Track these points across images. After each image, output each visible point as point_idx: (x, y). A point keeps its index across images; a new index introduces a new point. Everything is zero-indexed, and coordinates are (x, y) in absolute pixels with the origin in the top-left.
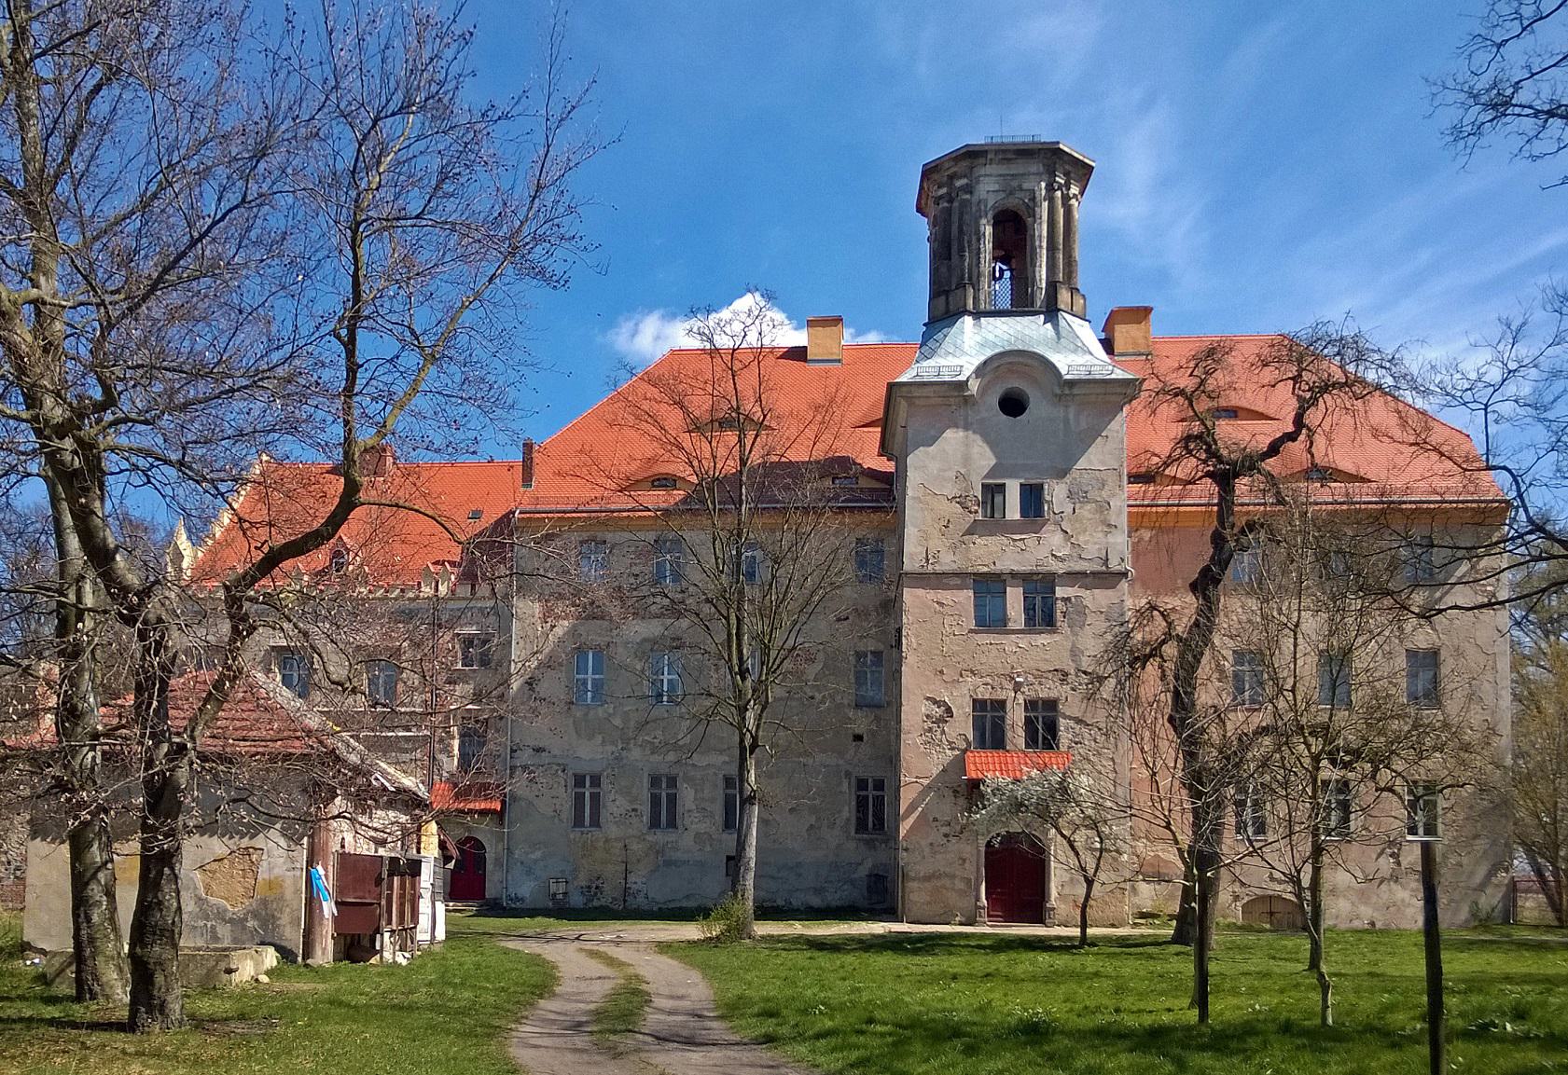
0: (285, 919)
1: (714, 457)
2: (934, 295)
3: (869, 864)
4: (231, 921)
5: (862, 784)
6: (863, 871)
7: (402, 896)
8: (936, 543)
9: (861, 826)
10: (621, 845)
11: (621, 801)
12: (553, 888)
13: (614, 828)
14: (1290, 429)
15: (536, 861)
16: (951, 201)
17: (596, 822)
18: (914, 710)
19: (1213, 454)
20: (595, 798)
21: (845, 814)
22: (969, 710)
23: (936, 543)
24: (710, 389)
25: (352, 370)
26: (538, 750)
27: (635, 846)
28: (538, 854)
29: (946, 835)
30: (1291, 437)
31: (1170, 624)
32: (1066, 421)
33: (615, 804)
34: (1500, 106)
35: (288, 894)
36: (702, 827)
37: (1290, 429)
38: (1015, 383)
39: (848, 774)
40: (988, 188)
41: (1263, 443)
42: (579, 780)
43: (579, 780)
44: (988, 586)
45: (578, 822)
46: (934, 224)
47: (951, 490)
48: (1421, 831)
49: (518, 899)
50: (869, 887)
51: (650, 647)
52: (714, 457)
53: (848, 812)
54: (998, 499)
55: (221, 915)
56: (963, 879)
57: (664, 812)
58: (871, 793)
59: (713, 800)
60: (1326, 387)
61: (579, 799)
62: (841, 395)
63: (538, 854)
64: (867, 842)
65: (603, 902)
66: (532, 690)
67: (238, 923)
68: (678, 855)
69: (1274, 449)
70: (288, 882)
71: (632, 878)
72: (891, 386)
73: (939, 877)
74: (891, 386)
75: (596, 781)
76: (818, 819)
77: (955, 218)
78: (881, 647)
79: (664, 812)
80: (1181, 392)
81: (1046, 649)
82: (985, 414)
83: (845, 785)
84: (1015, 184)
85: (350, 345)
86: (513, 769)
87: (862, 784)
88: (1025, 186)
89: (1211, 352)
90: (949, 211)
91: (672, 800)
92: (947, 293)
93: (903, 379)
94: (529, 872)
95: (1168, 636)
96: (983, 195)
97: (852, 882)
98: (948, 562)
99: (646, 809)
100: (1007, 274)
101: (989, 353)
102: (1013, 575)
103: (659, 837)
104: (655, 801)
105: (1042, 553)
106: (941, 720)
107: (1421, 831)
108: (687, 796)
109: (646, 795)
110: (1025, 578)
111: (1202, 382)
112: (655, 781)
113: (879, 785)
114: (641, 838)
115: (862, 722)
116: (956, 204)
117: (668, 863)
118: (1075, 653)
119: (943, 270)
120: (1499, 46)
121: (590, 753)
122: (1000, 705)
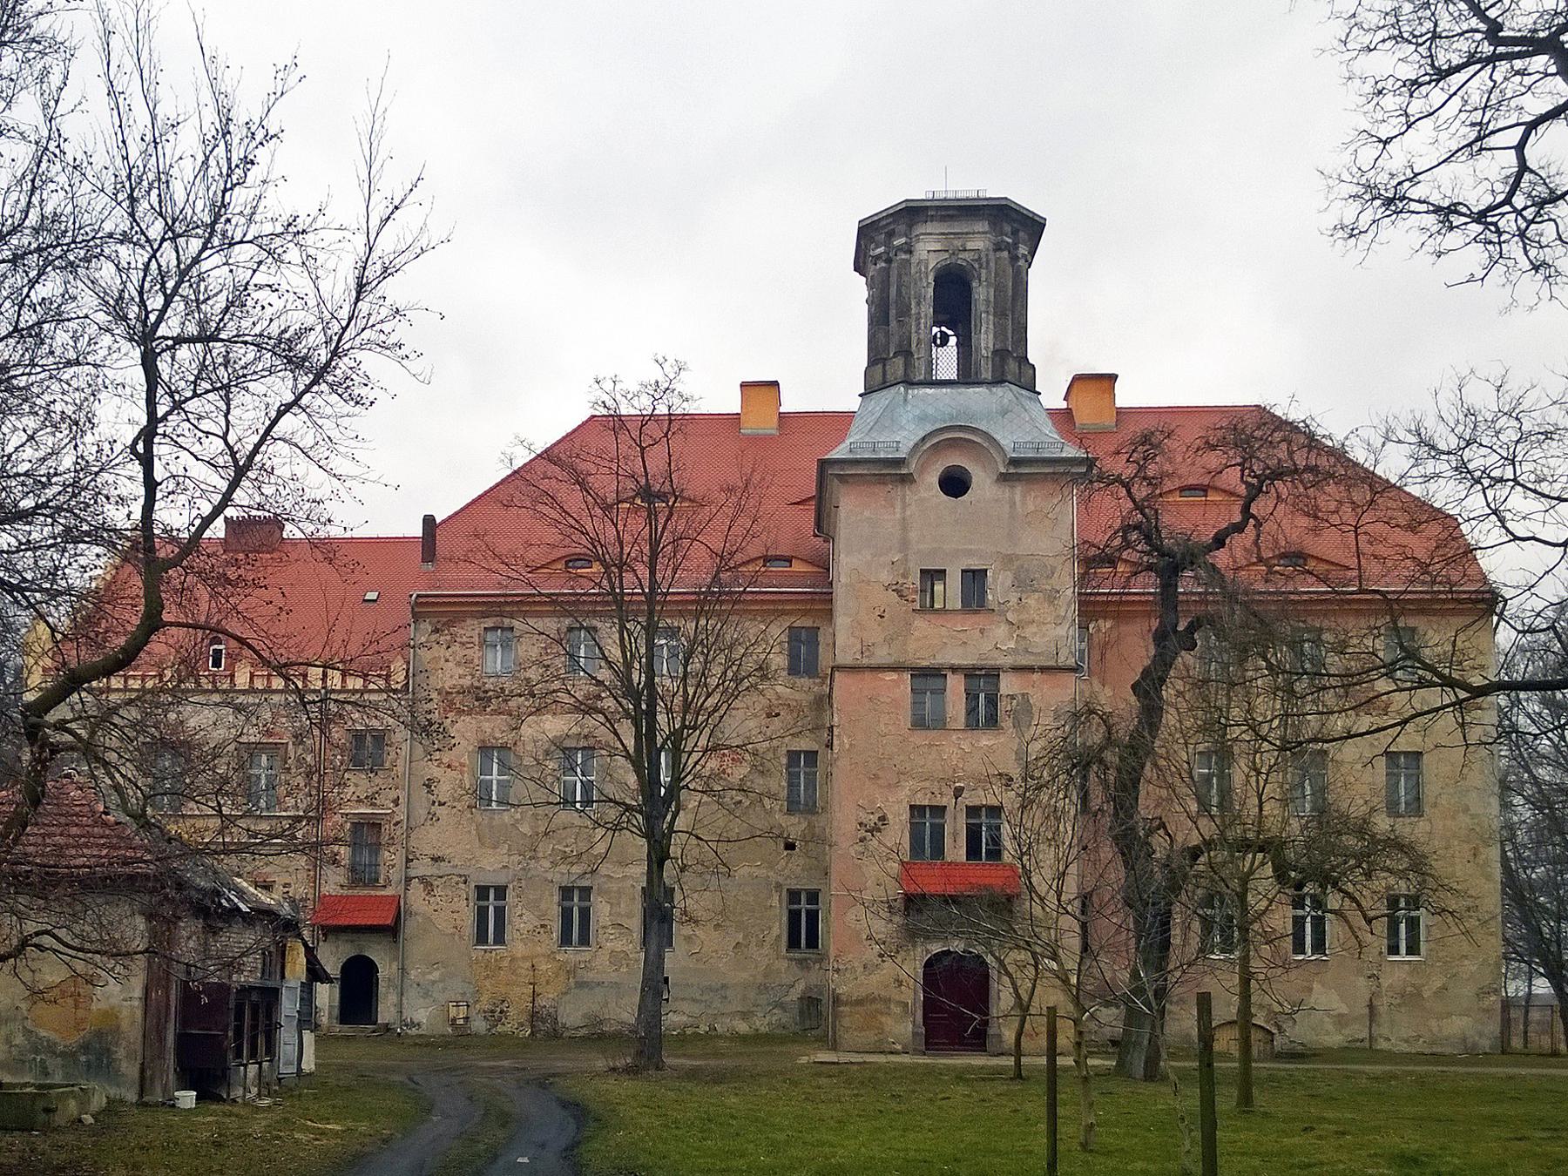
0: (121, 1053)
1: (621, 544)
2: (872, 362)
3: (800, 986)
4: (63, 1054)
5: (794, 896)
6: (795, 994)
7: (254, 1027)
8: (875, 634)
9: (793, 943)
10: (529, 964)
11: (527, 916)
12: (453, 1012)
13: (520, 946)
14: (1237, 518)
15: (434, 982)
16: (889, 261)
17: (500, 939)
18: (843, 818)
19: (1156, 548)
20: (500, 913)
21: (776, 931)
22: (906, 816)
23: (875, 634)
24: (614, 467)
25: (151, 485)
26: (436, 859)
27: (543, 966)
28: (436, 975)
29: (881, 956)
30: (1239, 528)
31: (1109, 728)
32: (1013, 504)
33: (521, 920)
34: (1395, 203)
35: (125, 1025)
36: (618, 946)
37: (1237, 518)
38: (955, 459)
39: (779, 886)
40: (929, 250)
41: (1208, 535)
42: (482, 892)
43: (482, 892)
44: (928, 676)
45: (481, 938)
46: (870, 286)
47: (886, 577)
48: (1403, 949)
49: (413, 1024)
50: (801, 1013)
51: (564, 750)
52: (621, 544)
53: (780, 928)
54: (938, 587)
55: (51, 1048)
56: (899, 1003)
57: (575, 925)
58: (804, 906)
59: (629, 916)
60: (1277, 474)
61: (482, 914)
62: (756, 478)
63: (436, 975)
64: (800, 962)
65: (508, 1028)
66: (430, 792)
67: (69, 1056)
68: (590, 976)
69: (1219, 542)
70: (125, 1013)
71: (541, 1002)
72: (823, 464)
73: (874, 1000)
74: (823, 464)
75: (501, 892)
76: (745, 937)
77: (894, 279)
78: (815, 747)
79: (575, 925)
80: (1118, 480)
81: (997, 749)
82: (924, 494)
83: (775, 901)
84: (958, 243)
85: (147, 461)
86: (408, 880)
87: (794, 896)
88: (970, 246)
89: (1146, 439)
90: (887, 271)
91: (585, 914)
92: (884, 361)
93: (839, 453)
94: (426, 994)
95: (1109, 740)
96: (924, 255)
97: (781, 1006)
98: (882, 655)
99: (556, 926)
100: (953, 340)
101: (929, 428)
102: (954, 669)
103: (571, 955)
104: (566, 915)
105: (986, 646)
106: (874, 830)
107: (1403, 949)
108: (601, 911)
109: (556, 911)
110: (970, 673)
111: (1141, 468)
112: (566, 892)
113: (813, 897)
114: (550, 957)
115: (795, 826)
116: (894, 265)
117: (581, 985)
118: (1021, 755)
119: (881, 336)
120: (1386, 143)
121: (491, 866)
122: (939, 811)
